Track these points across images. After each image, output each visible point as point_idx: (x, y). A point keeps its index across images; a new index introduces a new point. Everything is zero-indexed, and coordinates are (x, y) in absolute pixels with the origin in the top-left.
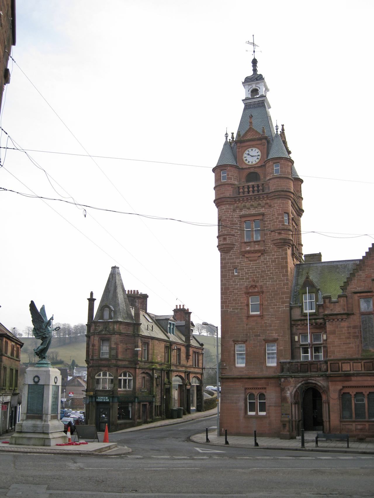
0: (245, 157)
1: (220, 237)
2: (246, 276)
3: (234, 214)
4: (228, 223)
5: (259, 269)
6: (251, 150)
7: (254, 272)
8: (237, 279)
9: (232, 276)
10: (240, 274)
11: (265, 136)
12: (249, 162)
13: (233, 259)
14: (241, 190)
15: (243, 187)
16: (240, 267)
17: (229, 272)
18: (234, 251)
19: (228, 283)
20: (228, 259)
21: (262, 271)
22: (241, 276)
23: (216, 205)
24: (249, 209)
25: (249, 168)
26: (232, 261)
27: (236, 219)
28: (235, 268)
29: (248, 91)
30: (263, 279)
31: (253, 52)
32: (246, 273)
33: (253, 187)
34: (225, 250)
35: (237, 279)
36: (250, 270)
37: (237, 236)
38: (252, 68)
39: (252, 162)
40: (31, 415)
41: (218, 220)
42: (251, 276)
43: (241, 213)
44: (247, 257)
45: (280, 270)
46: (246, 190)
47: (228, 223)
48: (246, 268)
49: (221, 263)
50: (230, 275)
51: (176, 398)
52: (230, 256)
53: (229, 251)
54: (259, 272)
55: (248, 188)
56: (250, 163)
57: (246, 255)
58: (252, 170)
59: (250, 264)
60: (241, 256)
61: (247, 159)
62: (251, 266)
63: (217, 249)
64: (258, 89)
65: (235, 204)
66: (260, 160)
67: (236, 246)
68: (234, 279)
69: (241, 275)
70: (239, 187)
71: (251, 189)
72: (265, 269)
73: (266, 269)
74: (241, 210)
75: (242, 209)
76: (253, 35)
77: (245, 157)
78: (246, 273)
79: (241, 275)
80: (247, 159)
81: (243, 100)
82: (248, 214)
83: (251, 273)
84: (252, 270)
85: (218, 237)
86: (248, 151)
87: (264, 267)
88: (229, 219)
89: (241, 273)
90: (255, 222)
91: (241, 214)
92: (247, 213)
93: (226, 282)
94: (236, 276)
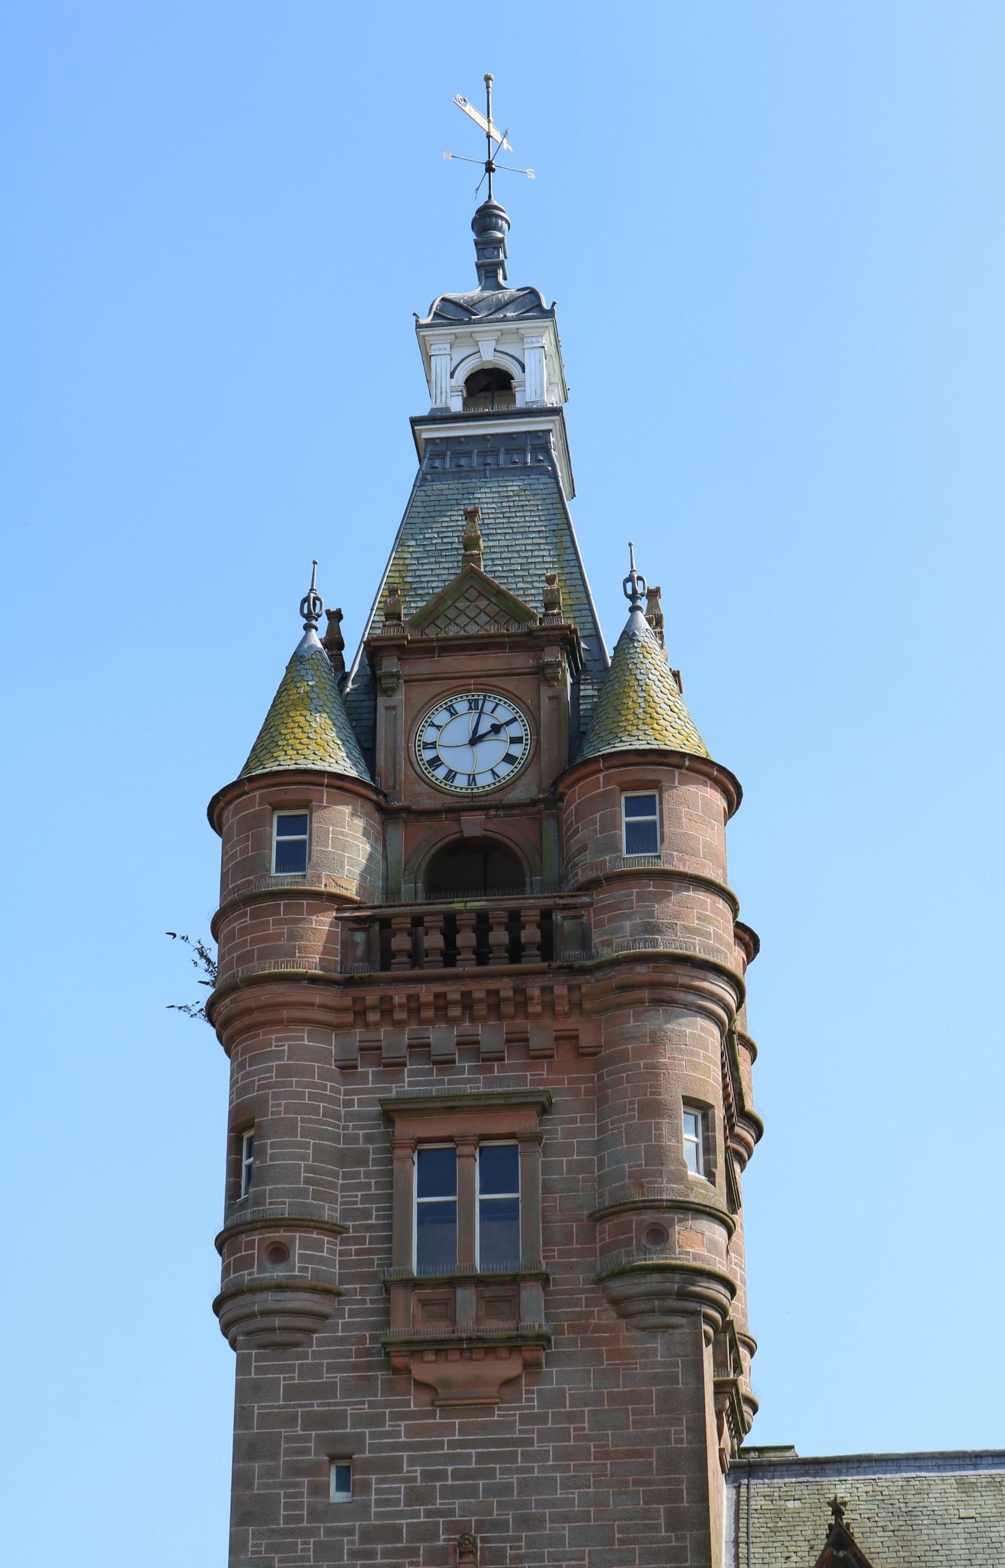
0: (426, 746)
1: (244, 1238)
2: (386, 1554)
3: (347, 1093)
4: (306, 1145)
5: (503, 1471)
6: (466, 705)
7: (473, 1492)
8: (350, 1532)
9: (315, 1514)
10: (373, 1497)
11: (561, 628)
12: (451, 775)
13: (327, 1391)
14: (401, 942)
15: (417, 921)
16: (373, 1448)
17: (295, 1485)
18: (337, 1341)
19: (297, 1431)
20: (292, 1392)
21: (525, 1486)
22: (379, 1516)
23: (220, 1037)
24: (446, 1063)
25: (454, 812)
26: (317, 1406)
27: (355, 1127)
28: (333, 1458)
29: (452, 376)
30: (531, 1542)
31: (484, 166)
32: (415, 1497)
33: (483, 922)
34: (274, 1329)
35: (350, 1532)
36: (442, 1475)
37: (361, 1240)
38: (471, 256)
39: (472, 779)
40: (573, 1562)
41: (231, 1130)
42: (451, 1512)
43: (390, 1090)
44: (421, 1385)
45: (650, 1483)
46: (435, 940)
47: (306, 1145)
48: (412, 1460)
49: (242, 1418)
50: (299, 1506)
51: (692, 983)
52: (307, 1371)
53: (298, 1337)
54: (505, 1489)
55: (450, 926)
56: (461, 782)
57: (424, 1370)
58: (473, 826)
59: (449, 1429)
60: (380, 1374)
61: (437, 759)
62: (452, 1444)
63: (214, 1322)
64: (514, 369)
65: (352, 1026)
66: (526, 767)
67: (346, 1303)
68: (329, 1531)
69: (379, 1503)
70: (385, 923)
71: (466, 939)
72: (587, 1438)
73: (554, 1468)
74: (394, 1067)
75: (404, 1065)
76: (488, 79)
77: (426, 746)
78: (415, 1497)
79: (379, 1503)
80: (437, 759)
81: (415, 422)
82: (439, 1094)
83: (449, 1492)
84: (457, 1475)
85: (222, 1243)
86: (448, 709)
87: (544, 1456)
88: (310, 1121)
89: (378, 1491)
90: (481, 1150)
91: (393, 1095)
92: (434, 1090)
93: (270, 1548)
94: (336, 1511)
